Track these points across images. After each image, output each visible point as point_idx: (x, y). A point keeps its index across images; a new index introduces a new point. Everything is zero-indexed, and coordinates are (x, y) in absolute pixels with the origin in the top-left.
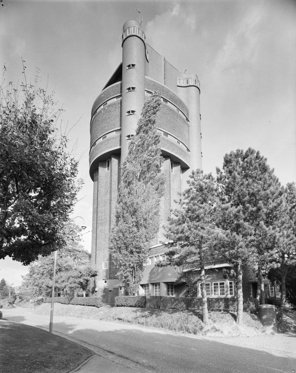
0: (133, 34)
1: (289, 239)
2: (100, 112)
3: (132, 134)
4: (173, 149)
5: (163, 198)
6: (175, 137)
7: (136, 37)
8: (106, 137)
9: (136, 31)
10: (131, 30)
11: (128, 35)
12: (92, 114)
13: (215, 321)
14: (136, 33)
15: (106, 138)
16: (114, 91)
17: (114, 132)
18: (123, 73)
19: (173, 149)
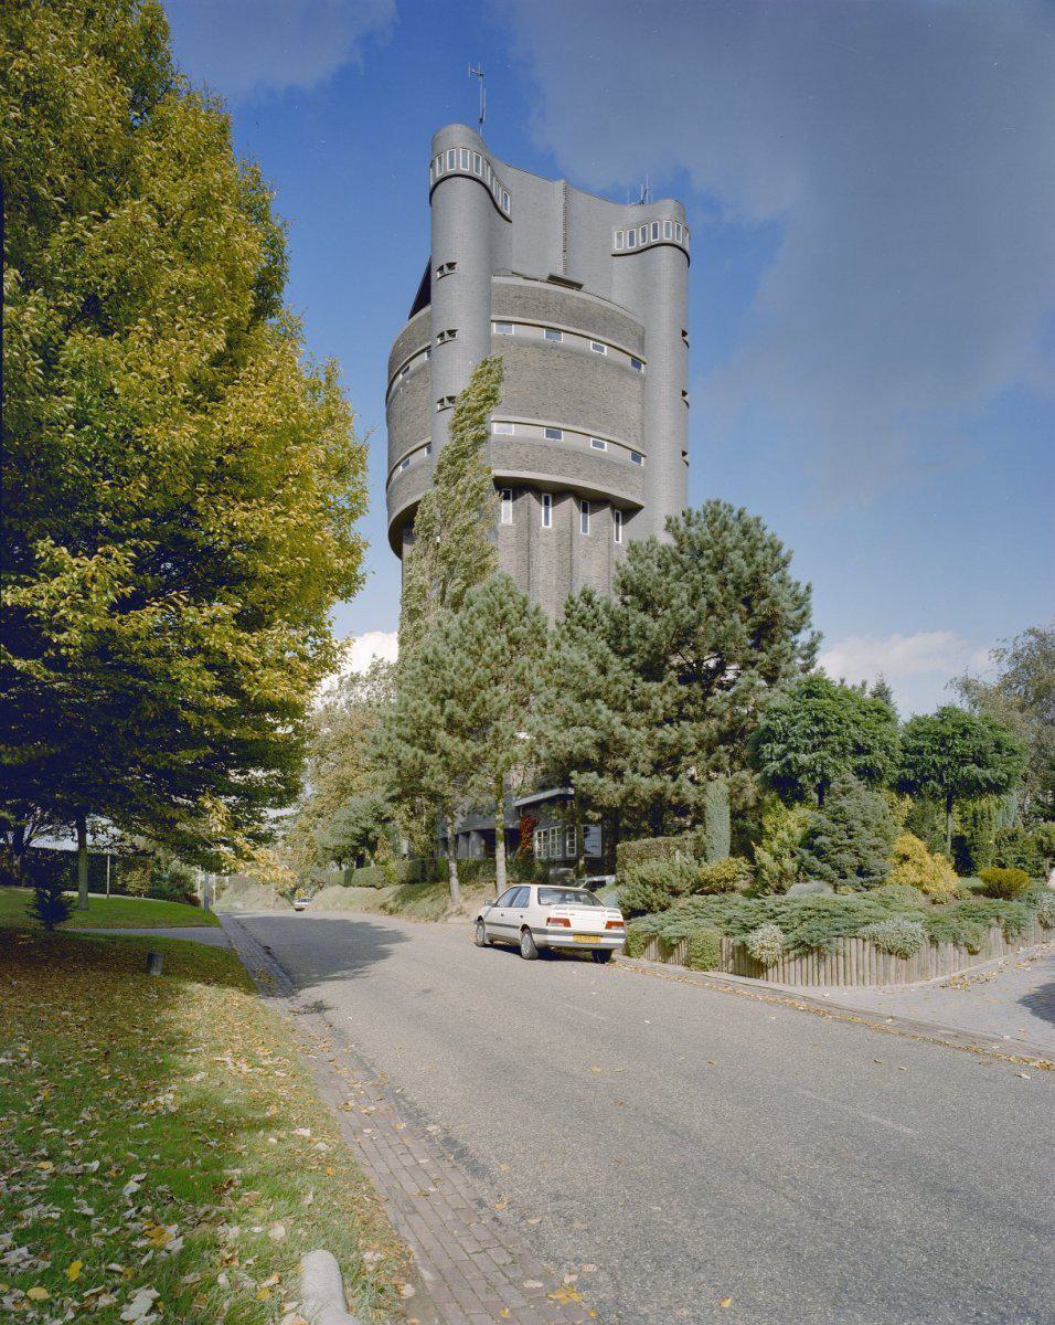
0: (450, 171)
1: (451, 846)
2: (397, 391)
3: (450, 395)
4: (578, 470)
5: (338, 889)
6: (621, 350)
7: (458, 178)
8: (408, 462)
9: (458, 161)
10: (445, 160)
11: (439, 175)
12: (390, 377)
13: (467, 899)
14: (458, 167)
15: (409, 372)
16: (422, 331)
17: (421, 356)
18: (432, 291)
19: (578, 470)
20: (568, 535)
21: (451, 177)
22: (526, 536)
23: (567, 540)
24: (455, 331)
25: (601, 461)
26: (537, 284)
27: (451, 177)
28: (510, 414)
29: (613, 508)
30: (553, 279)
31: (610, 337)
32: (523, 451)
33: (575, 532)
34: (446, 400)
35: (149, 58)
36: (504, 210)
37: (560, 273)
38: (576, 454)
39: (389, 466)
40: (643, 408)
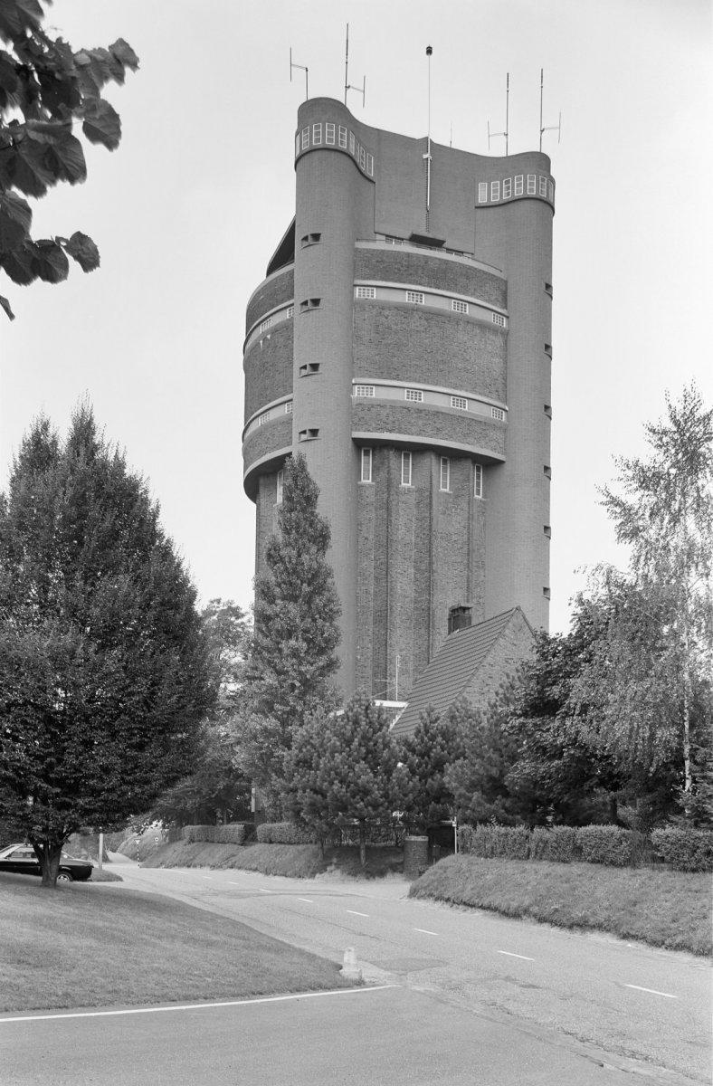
12: (247, 331)
20: (428, 493)
21: (315, 150)
22: (385, 495)
23: (426, 497)
24: (318, 430)
25: (461, 419)
26: (394, 247)
27: (315, 150)
28: (370, 377)
29: (474, 462)
30: (417, 240)
31: (472, 295)
32: (384, 413)
33: (434, 490)
34: (308, 367)
35: (484, 1002)
36: (367, 174)
37: (423, 232)
38: (437, 413)
39: (246, 420)
40: (506, 362)
